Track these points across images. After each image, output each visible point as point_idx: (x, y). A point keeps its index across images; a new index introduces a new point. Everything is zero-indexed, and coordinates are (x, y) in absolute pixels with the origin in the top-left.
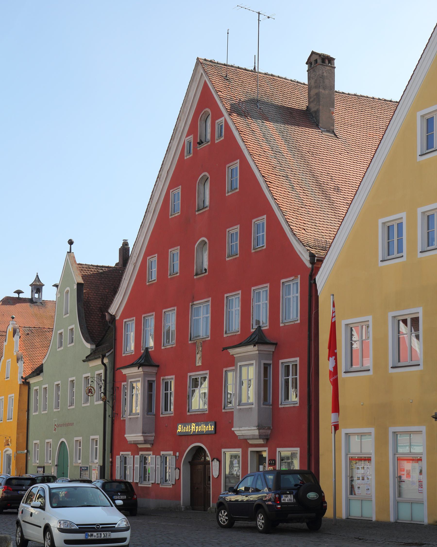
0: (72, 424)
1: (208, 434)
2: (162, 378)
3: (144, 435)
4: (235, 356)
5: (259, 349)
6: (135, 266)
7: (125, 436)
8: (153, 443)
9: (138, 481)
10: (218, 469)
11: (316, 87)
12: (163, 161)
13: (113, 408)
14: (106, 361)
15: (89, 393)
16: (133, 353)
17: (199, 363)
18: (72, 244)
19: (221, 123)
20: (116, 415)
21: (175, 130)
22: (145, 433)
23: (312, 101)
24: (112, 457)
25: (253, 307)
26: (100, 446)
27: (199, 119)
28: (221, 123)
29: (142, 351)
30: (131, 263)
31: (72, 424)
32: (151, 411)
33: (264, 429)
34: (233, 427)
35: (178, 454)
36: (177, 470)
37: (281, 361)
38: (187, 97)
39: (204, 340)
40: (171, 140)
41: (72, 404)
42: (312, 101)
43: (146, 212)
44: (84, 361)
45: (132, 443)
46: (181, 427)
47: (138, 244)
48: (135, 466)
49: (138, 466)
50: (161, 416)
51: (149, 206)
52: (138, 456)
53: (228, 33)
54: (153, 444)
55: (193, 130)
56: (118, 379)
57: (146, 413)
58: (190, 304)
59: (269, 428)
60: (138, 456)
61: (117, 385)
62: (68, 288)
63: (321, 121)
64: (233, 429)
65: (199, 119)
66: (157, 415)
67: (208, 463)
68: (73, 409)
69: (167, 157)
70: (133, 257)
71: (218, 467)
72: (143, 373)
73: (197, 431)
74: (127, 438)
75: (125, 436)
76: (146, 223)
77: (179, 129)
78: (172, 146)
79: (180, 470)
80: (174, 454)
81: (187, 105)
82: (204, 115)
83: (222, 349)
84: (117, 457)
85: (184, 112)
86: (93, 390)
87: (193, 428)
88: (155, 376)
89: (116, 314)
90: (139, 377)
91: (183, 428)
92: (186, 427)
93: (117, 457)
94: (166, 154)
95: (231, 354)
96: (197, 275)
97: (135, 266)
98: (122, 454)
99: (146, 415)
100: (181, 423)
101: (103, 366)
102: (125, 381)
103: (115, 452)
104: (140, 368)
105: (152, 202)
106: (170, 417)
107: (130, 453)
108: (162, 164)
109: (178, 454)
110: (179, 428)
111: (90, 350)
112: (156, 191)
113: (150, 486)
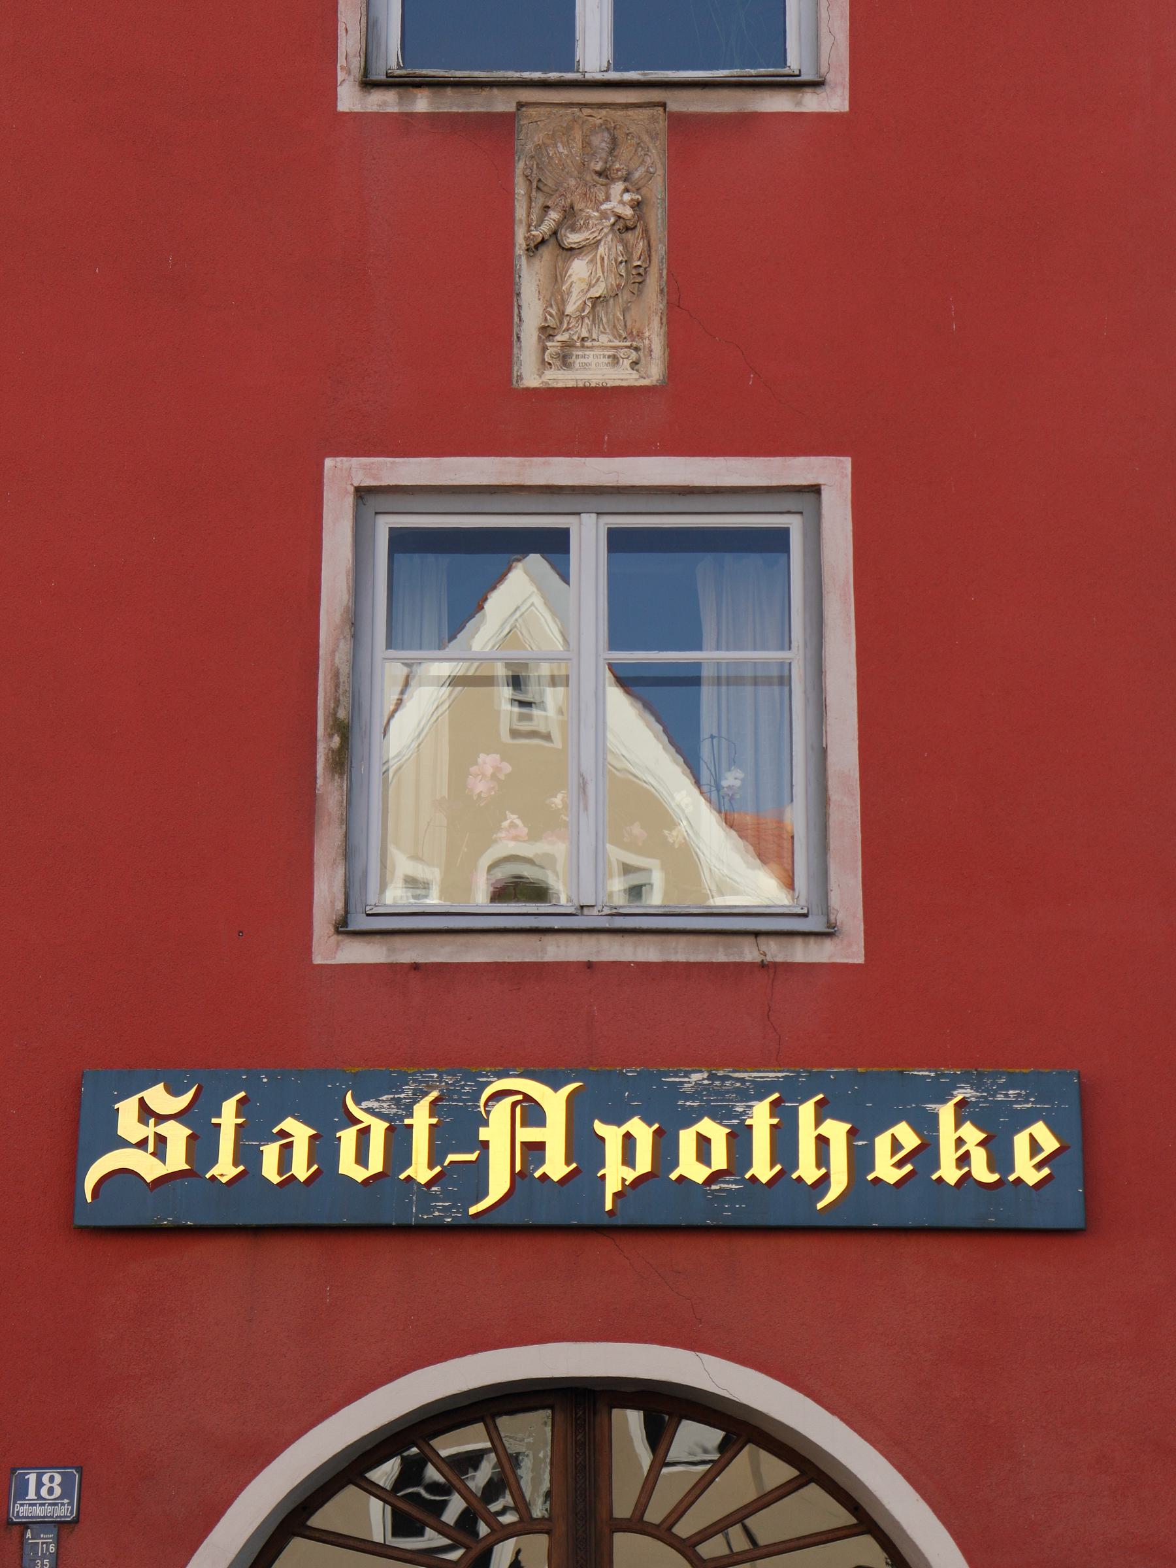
110: (128, 1123)
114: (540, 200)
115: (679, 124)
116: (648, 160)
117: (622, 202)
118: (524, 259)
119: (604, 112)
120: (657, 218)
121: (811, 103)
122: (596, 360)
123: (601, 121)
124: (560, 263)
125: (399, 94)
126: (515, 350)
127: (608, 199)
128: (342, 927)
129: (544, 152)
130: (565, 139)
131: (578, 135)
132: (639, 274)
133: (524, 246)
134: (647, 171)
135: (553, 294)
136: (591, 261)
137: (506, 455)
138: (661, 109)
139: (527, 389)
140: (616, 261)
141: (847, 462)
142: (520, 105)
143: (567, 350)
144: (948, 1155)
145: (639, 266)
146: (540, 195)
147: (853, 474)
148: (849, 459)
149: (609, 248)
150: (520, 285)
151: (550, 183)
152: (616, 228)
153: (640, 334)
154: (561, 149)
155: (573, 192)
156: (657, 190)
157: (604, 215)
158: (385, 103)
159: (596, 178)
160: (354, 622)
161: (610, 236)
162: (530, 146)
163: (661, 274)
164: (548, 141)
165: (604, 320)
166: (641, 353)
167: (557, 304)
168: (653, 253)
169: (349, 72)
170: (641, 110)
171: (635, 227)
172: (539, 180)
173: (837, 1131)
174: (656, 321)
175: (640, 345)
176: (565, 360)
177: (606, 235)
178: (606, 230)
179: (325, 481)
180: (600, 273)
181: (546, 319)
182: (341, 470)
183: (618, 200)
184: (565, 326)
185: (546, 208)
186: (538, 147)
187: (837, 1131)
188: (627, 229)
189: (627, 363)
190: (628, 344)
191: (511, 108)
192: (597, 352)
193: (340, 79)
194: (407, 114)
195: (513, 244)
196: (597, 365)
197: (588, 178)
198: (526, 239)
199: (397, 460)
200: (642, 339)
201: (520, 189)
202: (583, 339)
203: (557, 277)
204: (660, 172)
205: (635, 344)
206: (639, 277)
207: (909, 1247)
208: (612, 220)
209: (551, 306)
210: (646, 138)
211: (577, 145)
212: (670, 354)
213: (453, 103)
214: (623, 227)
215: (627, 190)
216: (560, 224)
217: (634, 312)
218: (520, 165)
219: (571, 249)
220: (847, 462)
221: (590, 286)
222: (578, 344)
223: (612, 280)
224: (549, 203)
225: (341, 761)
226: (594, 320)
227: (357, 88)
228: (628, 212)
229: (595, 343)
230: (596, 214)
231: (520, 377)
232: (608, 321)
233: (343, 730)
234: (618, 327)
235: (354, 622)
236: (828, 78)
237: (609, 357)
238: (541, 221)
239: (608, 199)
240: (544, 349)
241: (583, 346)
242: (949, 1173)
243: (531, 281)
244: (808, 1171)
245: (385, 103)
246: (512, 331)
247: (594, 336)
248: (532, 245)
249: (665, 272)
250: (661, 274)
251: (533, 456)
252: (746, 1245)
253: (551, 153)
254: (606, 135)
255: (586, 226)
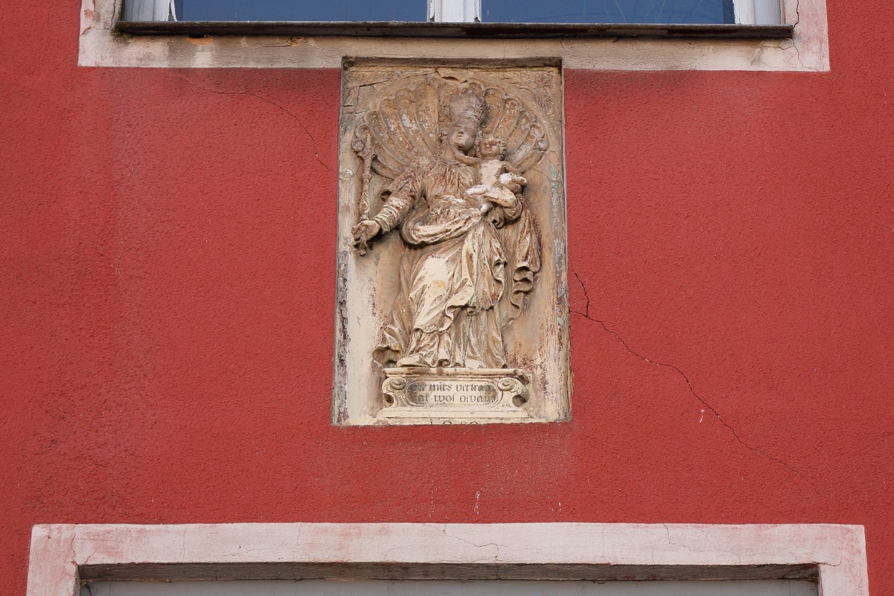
114: (376, 186)
115: (580, 85)
116: (537, 134)
117: (499, 185)
118: (351, 259)
119: (470, 74)
120: (551, 209)
121: (774, 59)
122: (461, 393)
123: (465, 85)
124: (406, 266)
125: (169, 43)
126: (337, 378)
127: (477, 181)
129: (383, 124)
130: (413, 109)
131: (432, 103)
132: (525, 280)
133: (352, 241)
134: (536, 148)
135: (394, 307)
136: (453, 260)
137: (321, 520)
138: (554, 71)
139: (355, 428)
140: (490, 261)
141: (859, 532)
142: (349, 62)
143: (415, 379)
145: (525, 269)
146: (376, 179)
147: (868, 548)
148: (862, 528)
149: (479, 243)
150: (345, 290)
151: (391, 164)
152: (490, 219)
153: (527, 362)
154: (407, 123)
155: (424, 175)
156: (550, 174)
157: (472, 202)
158: (149, 57)
159: (460, 154)
161: (481, 229)
162: (362, 115)
163: (558, 279)
164: (388, 111)
165: (473, 341)
166: (529, 387)
167: (401, 320)
168: (546, 253)
169: (97, 18)
170: (524, 71)
171: (518, 219)
172: (375, 159)
174: (552, 343)
175: (528, 375)
176: (413, 394)
177: (475, 226)
178: (475, 220)
179: (32, 557)
180: (466, 275)
181: (384, 340)
182: (58, 541)
183: (493, 182)
184: (413, 345)
185: (386, 194)
186: (374, 115)
188: (508, 222)
189: (508, 397)
190: (510, 370)
191: (336, 63)
192: (462, 382)
193: (83, 27)
194: (180, 70)
195: (335, 237)
196: (463, 399)
197: (448, 156)
198: (355, 231)
199: (148, 527)
200: (531, 368)
201: (347, 167)
202: (441, 363)
203: (400, 285)
204: (554, 147)
205: (520, 371)
206: (525, 282)
208: (485, 207)
209: (392, 322)
210: (533, 105)
211: (431, 119)
212: (575, 381)
213: (249, 56)
214: (502, 219)
215: (505, 170)
216: (406, 214)
217: (519, 333)
218: (347, 138)
219: (423, 245)
220: (859, 532)
221: (452, 292)
222: (434, 370)
223: (486, 287)
224: (390, 188)
226: (457, 339)
227: (109, 37)
228: (507, 197)
229: (459, 370)
230: (460, 201)
231: (344, 415)
232: (479, 342)
234: (495, 351)
236: (797, 30)
237: (481, 388)
238: (378, 210)
239: (477, 181)
240: (382, 378)
241: (441, 374)
243: (362, 290)
245: (149, 57)
246: (332, 349)
247: (459, 359)
248: (364, 239)
249: (564, 276)
250: (558, 279)
251: (363, 521)
253: (393, 127)
254: (474, 100)
255: (445, 214)
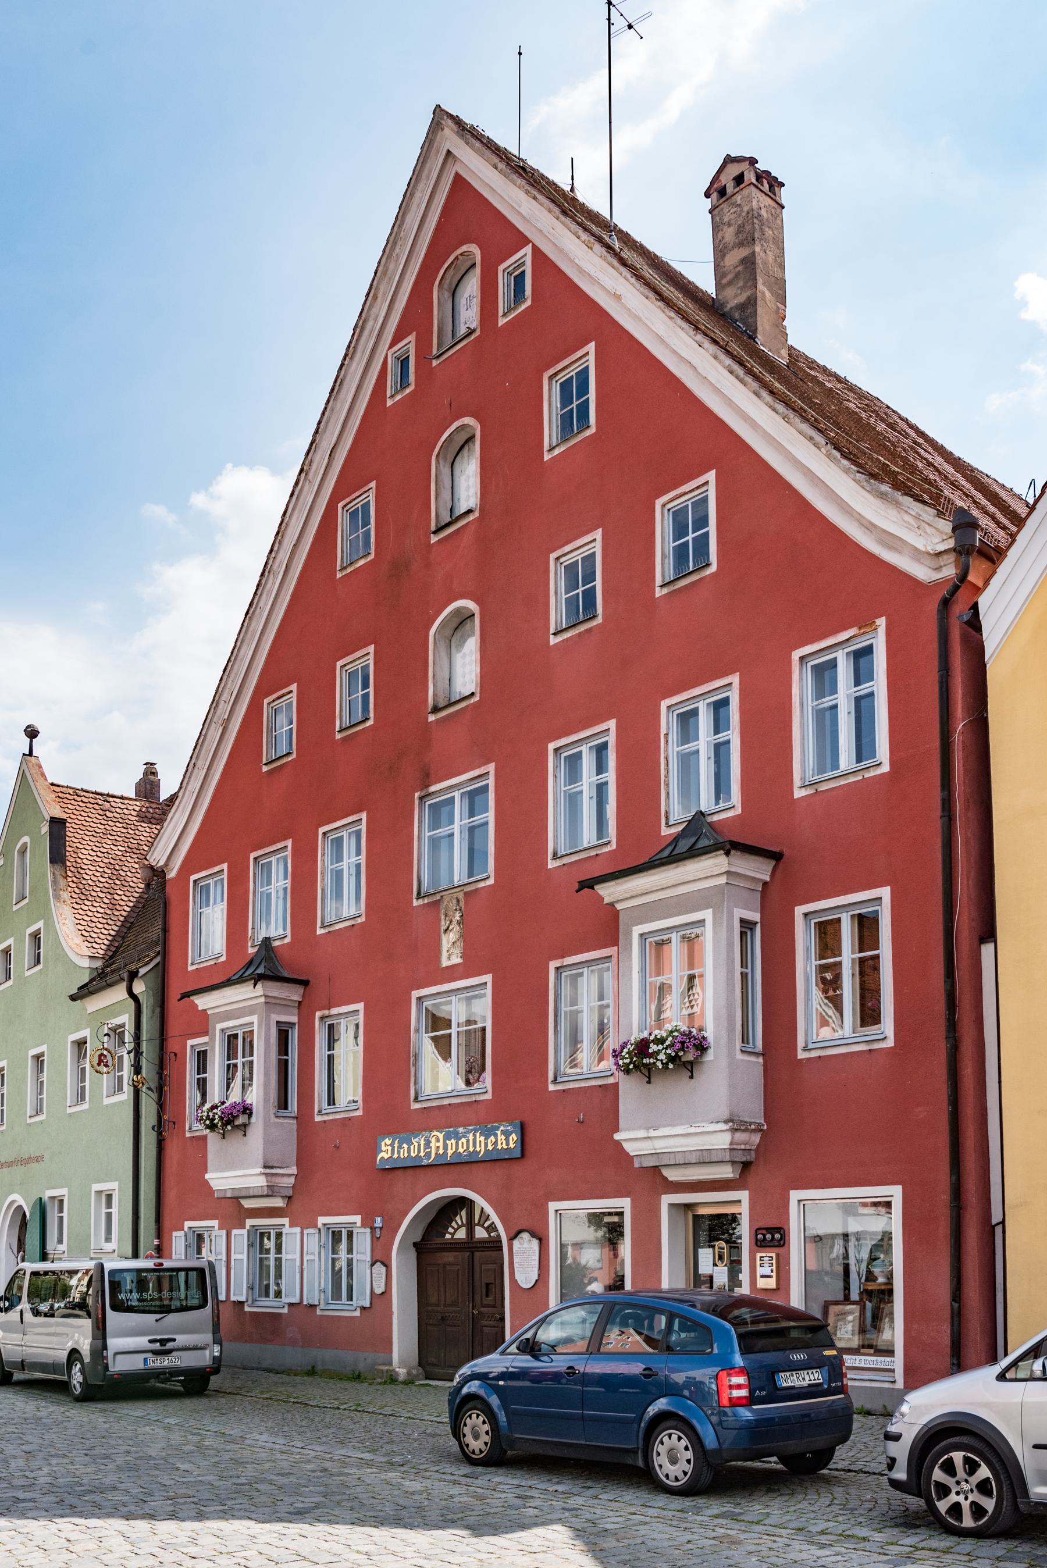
0: (39, 1159)
1: (495, 1160)
2: (318, 1014)
3: (268, 1171)
4: (619, 907)
5: (733, 869)
6: (225, 729)
7: (207, 1176)
8: (290, 1193)
9: (243, 1299)
10: (537, 1262)
11: (741, 244)
12: (319, 423)
13: (161, 1105)
14: (139, 987)
15: (99, 1064)
16: (223, 959)
17: (451, 954)
18: (36, 736)
19: (519, 266)
20: (171, 1124)
21: (359, 328)
22: (272, 1167)
23: (730, 283)
24: (159, 1235)
25: (667, 759)
26: (121, 1210)
27: (437, 283)
28: (519, 266)
29: (251, 951)
30: (215, 720)
31: (39, 1159)
32: (286, 1108)
33: (746, 1130)
34: (617, 1130)
35: (378, 1222)
36: (380, 1269)
37: (800, 910)
38: (400, 227)
39: (468, 889)
40: (345, 359)
41: (38, 1111)
42: (730, 283)
43: (263, 574)
44: (73, 998)
45: (229, 1195)
46: (392, 1145)
47: (236, 667)
48: (233, 1257)
49: (244, 1257)
50: (318, 1118)
51: (273, 555)
52: (244, 1232)
53: (520, 54)
54: (290, 1198)
55: (415, 318)
56: (174, 1027)
57: (272, 1111)
58: (417, 795)
59: (758, 1129)
60: (244, 1232)
61: (172, 1046)
62: (26, 839)
63: (760, 329)
64: (617, 1137)
65: (437, 283)
66: (304, 1119)
67: (495, 1245)
68: (41, 1122)
69: (332, 410)
70: (222, 703)
71: (537, 1257)
72: (263, 1000)
73: (450, 1152)
74: (212, 1183)
75: (207, 1176)
76: (261, 604)
77: (370, 324)
78: (348, 378)
79: (387, 1265)
80: (368, 1222)
81: (397, 251)
82: (451, 272)
83: (577, 886)
84: (175, 1234)
85: (389, 273)
86: (109, 1057)
87: (436, 1144)
88: (296, 1011)
89: (166, 864)
90: (251, 1014)
91: (400, 1147)
92: (410, 1143)
93: (175, 1234)
94: (328, 401)
95: (606, 901)
96: (436, 710)
97: (225, 729)
98: (190, 1228)
99: (272, 1116)
100: (389, 1133)
101: (131, 1002)
102: (205, 1033)
103: (167, 1223)
104: (259, 985)
105: (280, 543)
106: (350, 1119)
107: (215, 1223)
108: (317, 432)
109: (378, 1222)
110: (384, 1148)
111: (87, 972)
112: (293, 509)
113: (285, 1310)
121: (359, 920)
128: (416, 1099)
144: (499, 1143)
160: (417, 1031)
173: (482, 1138)
187: (482, 1138)
201: (443, 917)
207: (498, 1164)
225: (415, 1065)
233: (416, 1056)
235: (417, 1031)
242: (499, 1147)
244: (478, 1149)
252: (474, 1165)
